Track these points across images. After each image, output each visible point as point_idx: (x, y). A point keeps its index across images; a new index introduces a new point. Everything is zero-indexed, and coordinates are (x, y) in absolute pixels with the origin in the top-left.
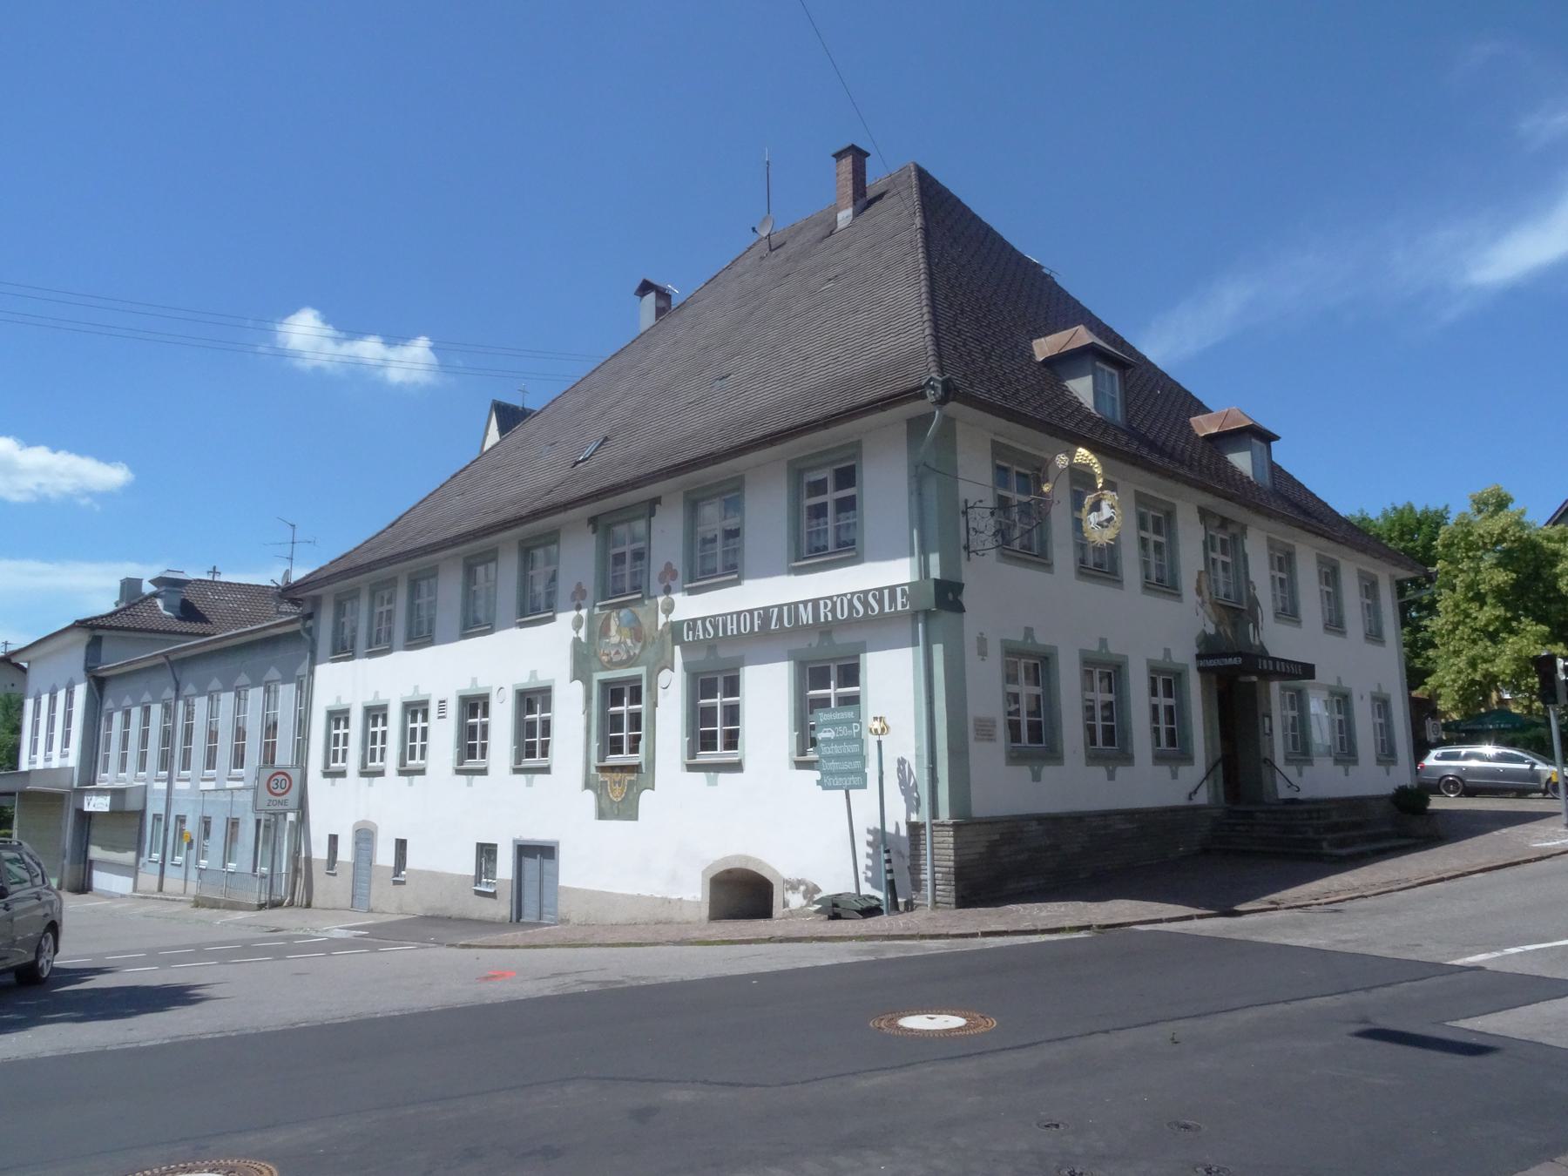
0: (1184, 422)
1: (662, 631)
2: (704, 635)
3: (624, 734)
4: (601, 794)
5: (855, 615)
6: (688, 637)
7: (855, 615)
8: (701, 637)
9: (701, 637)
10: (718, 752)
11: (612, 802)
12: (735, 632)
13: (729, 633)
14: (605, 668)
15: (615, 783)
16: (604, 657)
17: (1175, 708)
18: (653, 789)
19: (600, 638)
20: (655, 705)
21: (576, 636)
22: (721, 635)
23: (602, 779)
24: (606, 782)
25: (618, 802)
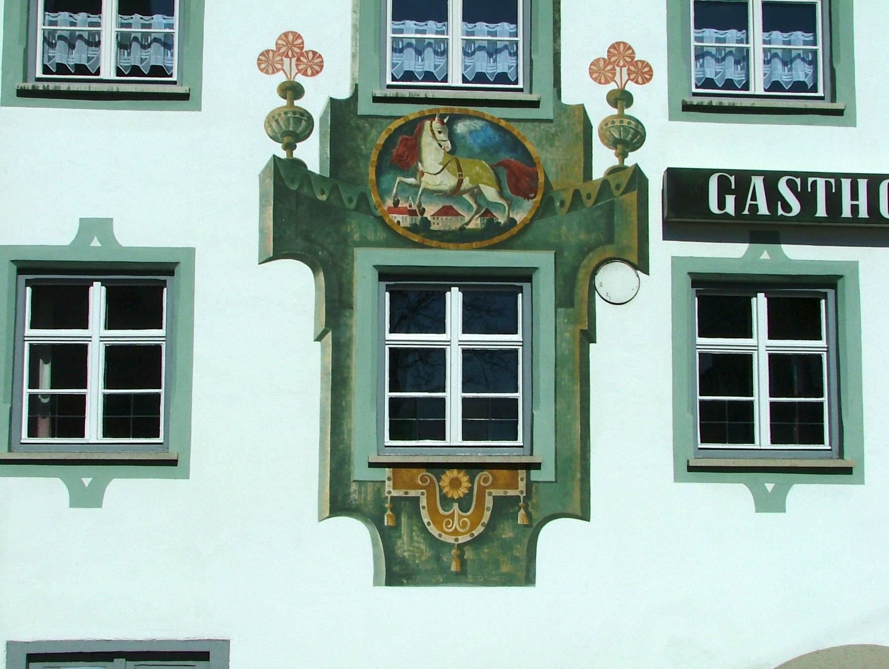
0: (294, 113)
1: (605, 183)
2: (771, 206)
3: (727, 422)
4: (397, 527)
5: (780, 212)
6: (721, 204)
7: (780, 212)
8: (763, 210)
9: (763, 210)
10: (388, 394)
11: (435, 543)
12: (863, 213)
13: (846, 212)
14: (396, 239)
15: (446, 501)
16: (398, 217)
17: (697, 335)
18: (585, 515)
19: (379, 172)
20: (589, 336)
21: (283, 154)
22: (821, 211)
23: (395, 493)
24: (417, 499)
25: (461, 547)
